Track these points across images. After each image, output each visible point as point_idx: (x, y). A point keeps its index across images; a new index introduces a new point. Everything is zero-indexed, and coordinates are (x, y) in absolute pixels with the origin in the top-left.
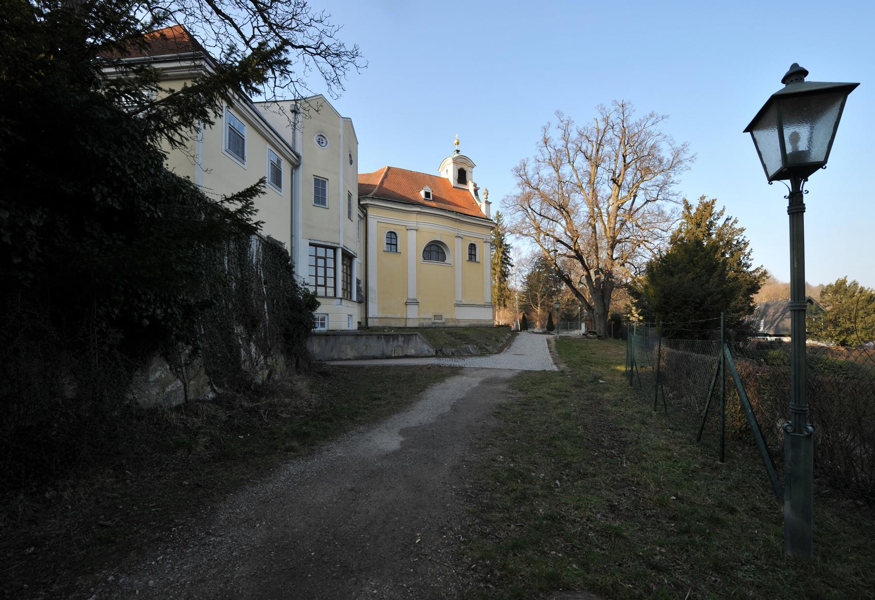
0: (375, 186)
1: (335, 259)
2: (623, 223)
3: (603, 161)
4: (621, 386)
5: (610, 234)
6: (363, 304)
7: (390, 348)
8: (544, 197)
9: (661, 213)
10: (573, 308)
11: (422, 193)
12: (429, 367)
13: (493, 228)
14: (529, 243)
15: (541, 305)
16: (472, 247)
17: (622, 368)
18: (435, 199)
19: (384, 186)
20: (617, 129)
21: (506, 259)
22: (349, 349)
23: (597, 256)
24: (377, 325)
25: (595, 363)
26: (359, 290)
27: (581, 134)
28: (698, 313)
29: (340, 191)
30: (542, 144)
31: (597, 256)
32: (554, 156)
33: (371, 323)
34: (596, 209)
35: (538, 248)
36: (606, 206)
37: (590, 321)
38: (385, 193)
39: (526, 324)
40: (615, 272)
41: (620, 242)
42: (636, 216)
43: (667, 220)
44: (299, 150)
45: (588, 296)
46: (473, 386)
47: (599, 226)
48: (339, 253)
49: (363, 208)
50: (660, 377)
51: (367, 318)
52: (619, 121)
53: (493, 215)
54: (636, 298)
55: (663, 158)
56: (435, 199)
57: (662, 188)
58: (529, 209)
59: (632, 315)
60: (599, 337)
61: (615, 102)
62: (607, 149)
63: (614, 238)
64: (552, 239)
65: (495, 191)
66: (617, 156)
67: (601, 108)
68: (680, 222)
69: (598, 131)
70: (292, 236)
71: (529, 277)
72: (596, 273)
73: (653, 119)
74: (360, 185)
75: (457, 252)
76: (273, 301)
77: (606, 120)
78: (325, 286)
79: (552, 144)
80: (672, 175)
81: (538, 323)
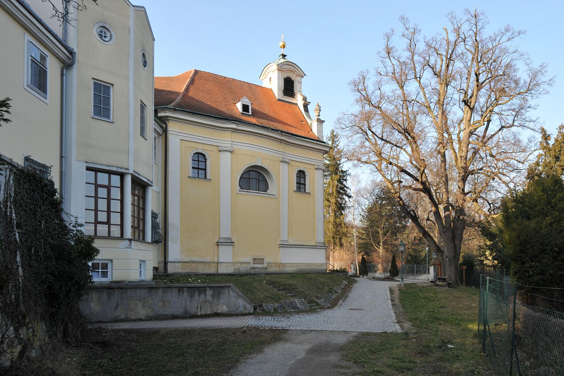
0: (178, 94)
1: (122, 188)
2: (476, 152)
3: (454, 78)
4: (473, 351)
5: (461, 164)
6: (161, 245)
7: (195, 304)
8: (386, 117)
9: (517, 143)
10: (420, 248)
11: (239, 106)
12: (244, 331)
13: (326, 152)
14: (368, 171)
15: (385, 243)
16: (301, 174)
17: (474, 327)
18: (255, 114)
19: (191, 94)
20: (470, 42)
21: (342, 189)
22: (140, 306)
23: (447, 189)
24: (180, 271)
25: (444, 320)
26: (155, 226)
27: (429, 46)
28: (557, 263)
29: (129, 99)
30: (384, 54)
31: (447, 189)
32: (398, 70)
33: (171, 269)
34: (446, 135)
35: (379, 178)
36: (457, 132)
37: (439, 266)
38: (189, 103)
39: (366, 268)
40: (466, 209)
41: (472, 173)
42: (491, 144)
43: (524, 151)
44: (72, 43)
45: (435, 235)
46: (300, 357)
47: (449, 154)
48: (128, 181)
49: (162, 122)
50: (515, 340)
51: (166, 263)
52: (471, 33)
53: (326, 136)
54: (490, 240)
55: (519, 79)
56: (255, 114)
57: (518, 113)
58: (368, 132)
59: (486, 258)
60: (449, 285)
61: (467, 11)
62: (458, 64)
63: (465, 169)
64: (395, 168)
65: (329, 106)
66: (469, 73)
67: (452, 17)
68: (537, 153)
69: (448, 43)
70: (61, 157)
71: (370, 210)
72: (446, 209)
73: (509, 34)
74: (158, 93)
75: (282, 180)
76: (30, 250)
77: (457, 31)
78: (108, 223)
79: (396, 55)
80: (529, 98)
81: (380, 266)
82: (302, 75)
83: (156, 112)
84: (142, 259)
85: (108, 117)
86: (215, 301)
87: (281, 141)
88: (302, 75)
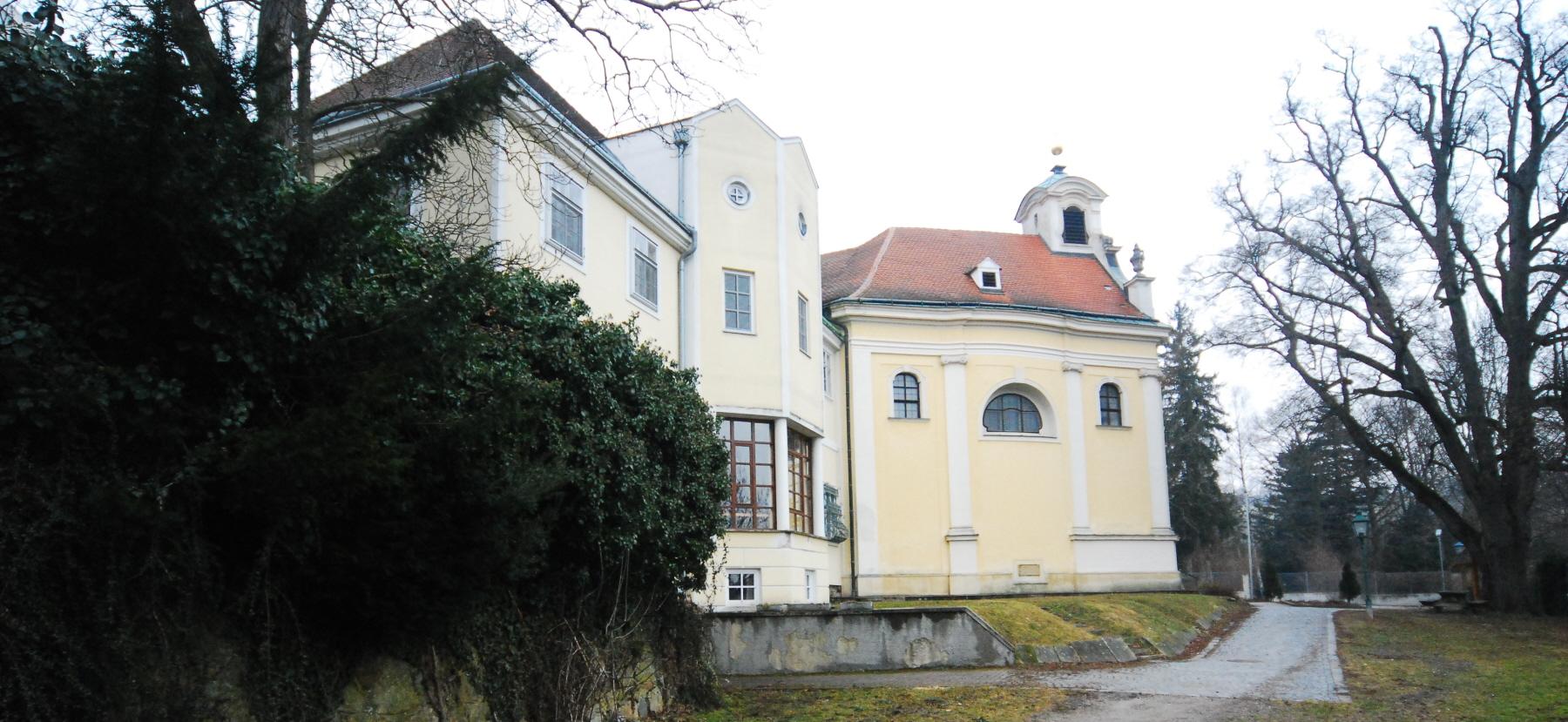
6: (845, 545)
16: (1110, 392)
26: (831, 513)
44: (692, 221)
49: (839, 327)
51: (854, 578)
65: (1175, 251)
75: (1071, 405)
82: (1098, 196)
83: (826, 311)
84: (810, 567)
85: (749, 328)
86: (938, 637)
87: (1062, 331)
88: (1098, 196)
